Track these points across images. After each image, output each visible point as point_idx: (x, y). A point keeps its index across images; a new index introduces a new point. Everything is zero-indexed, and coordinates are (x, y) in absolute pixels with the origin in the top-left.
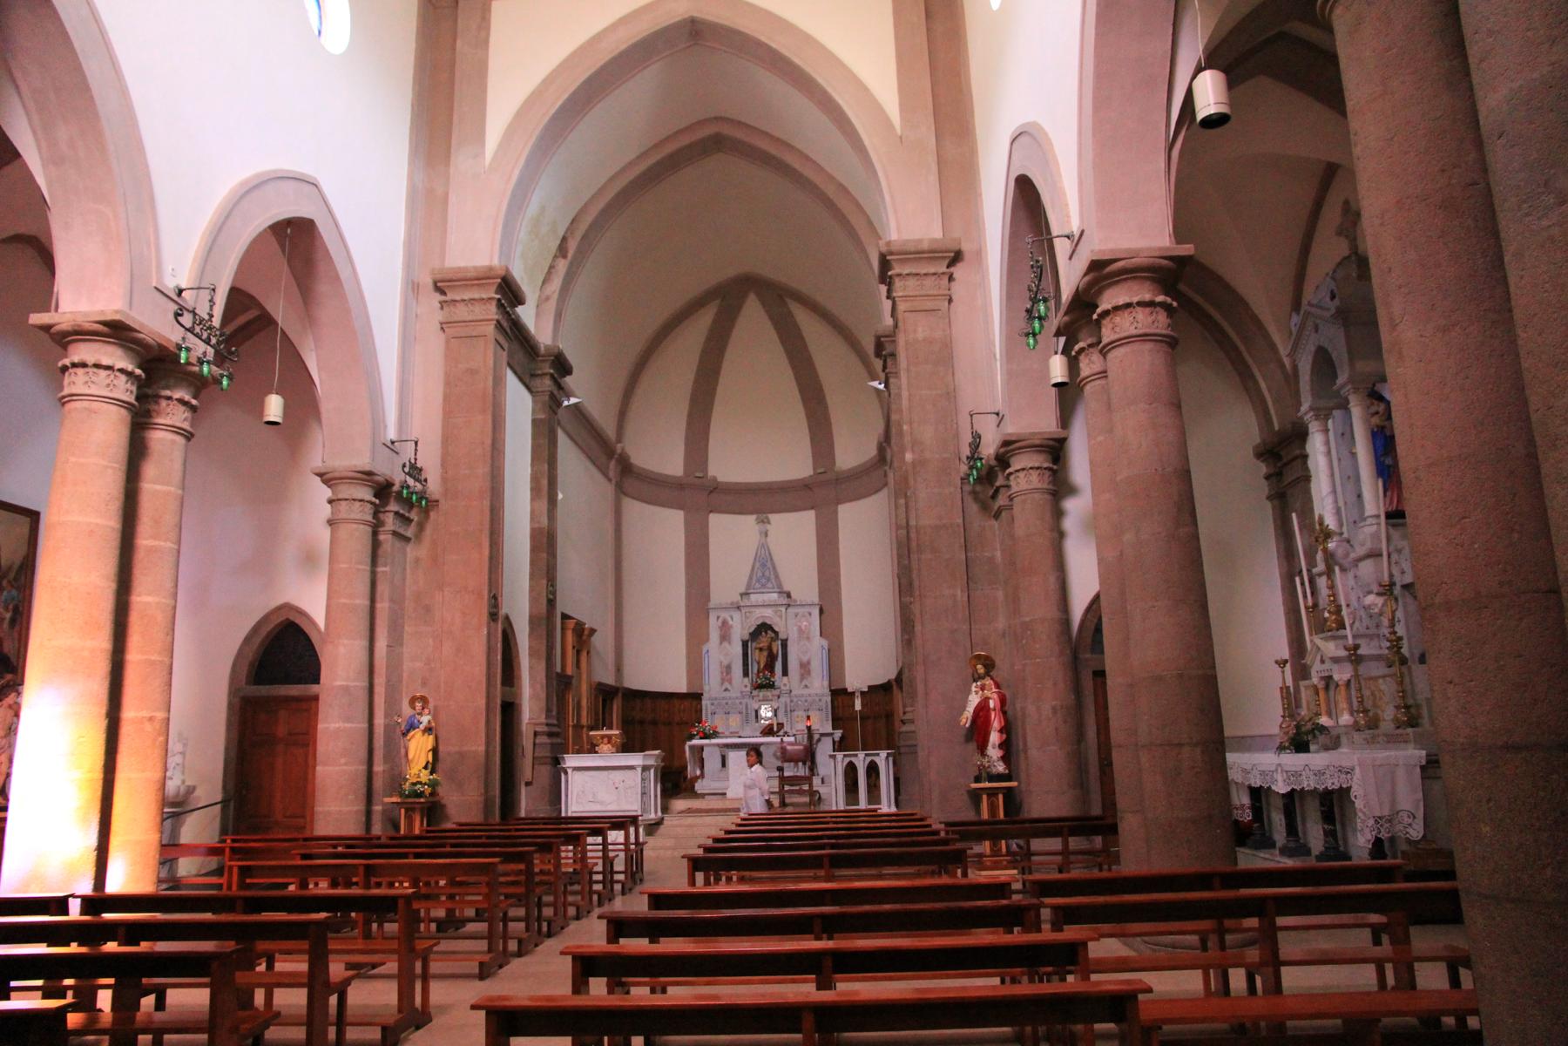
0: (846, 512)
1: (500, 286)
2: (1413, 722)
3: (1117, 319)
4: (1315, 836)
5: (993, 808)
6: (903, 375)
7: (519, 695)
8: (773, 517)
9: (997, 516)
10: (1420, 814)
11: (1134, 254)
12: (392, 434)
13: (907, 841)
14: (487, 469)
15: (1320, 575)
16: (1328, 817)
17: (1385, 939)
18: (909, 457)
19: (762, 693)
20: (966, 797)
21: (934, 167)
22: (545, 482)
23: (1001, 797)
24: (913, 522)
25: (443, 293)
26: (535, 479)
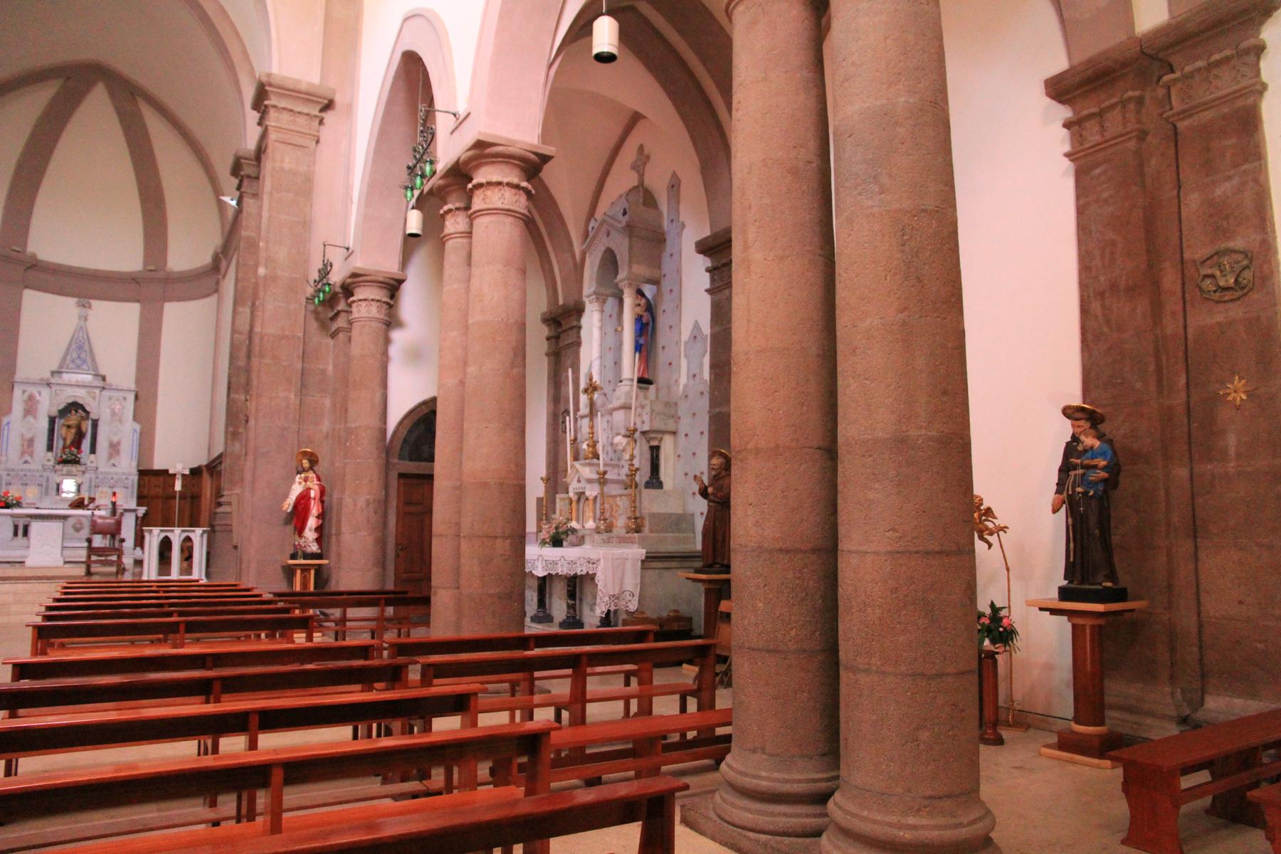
2: (638, 530)
3: (489, 193)
4: (559, 608)
5: (305, 584)
6: (266, 198)
8: (95, 303)
9: (334, 335)
11: (511, 143)
13: (220, 609)
15: (582, 417)
16: (572, 595)
17: (634, 681)
18: (261, 271)
19: (66, 468)
20: (280, 571)
21: (321, 21)
23: (313, 572)
24: (257, 329)
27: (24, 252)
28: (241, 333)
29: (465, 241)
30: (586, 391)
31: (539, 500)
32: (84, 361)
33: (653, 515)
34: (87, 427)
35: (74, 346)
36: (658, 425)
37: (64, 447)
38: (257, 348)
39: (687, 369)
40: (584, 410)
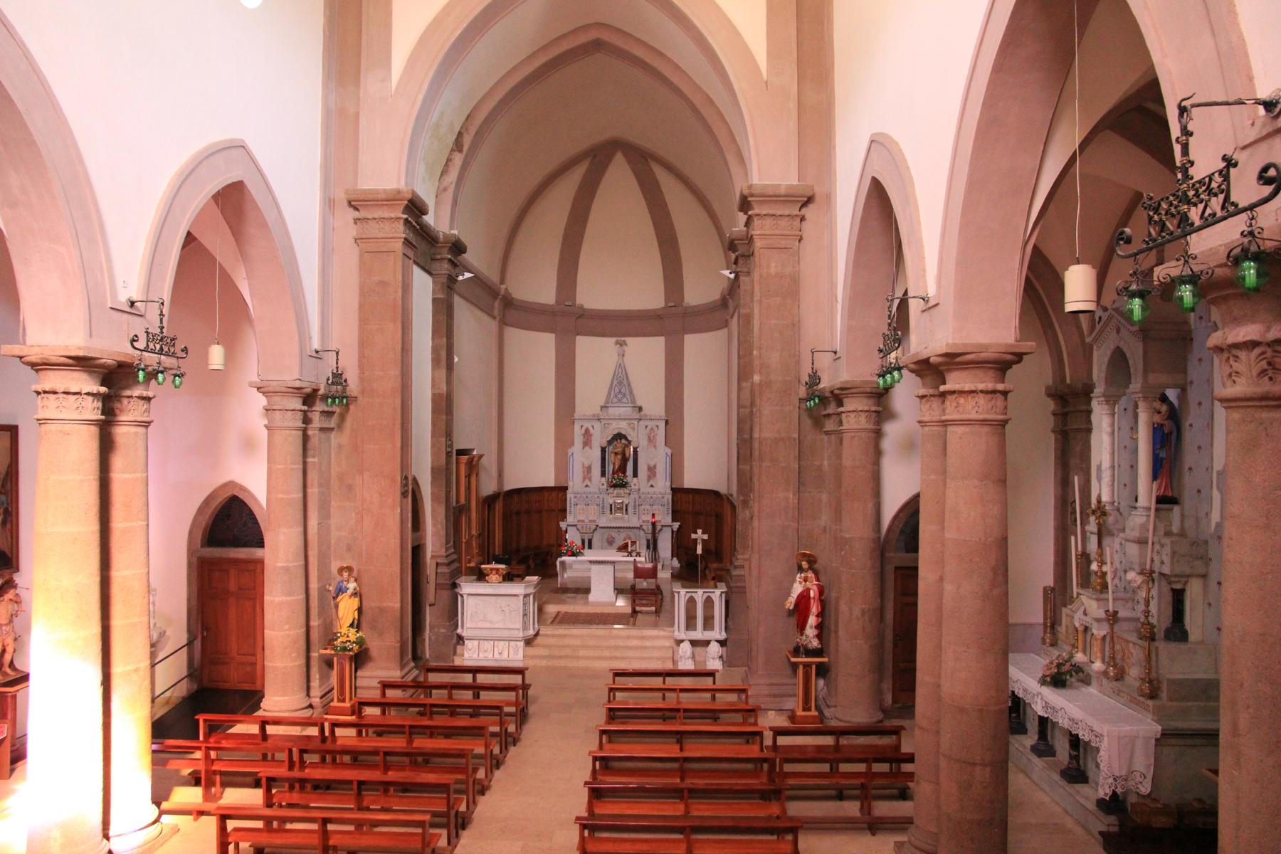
0: (693, 343)
1: (407, 206)
2: (1153, 695)
3: (962, 400)
7: (423, 537)
10: (1150, 777)
11: (985, 348)
12: (316, 344)
14: (398, 372)
18: (756, 378)
19: (617, 491)
22: (443, 354)
25: (356, 209)
26: (435, 350)
27: (574, 305)
28: (744, 407)
32: (624, 395)
33: (1172, 682)
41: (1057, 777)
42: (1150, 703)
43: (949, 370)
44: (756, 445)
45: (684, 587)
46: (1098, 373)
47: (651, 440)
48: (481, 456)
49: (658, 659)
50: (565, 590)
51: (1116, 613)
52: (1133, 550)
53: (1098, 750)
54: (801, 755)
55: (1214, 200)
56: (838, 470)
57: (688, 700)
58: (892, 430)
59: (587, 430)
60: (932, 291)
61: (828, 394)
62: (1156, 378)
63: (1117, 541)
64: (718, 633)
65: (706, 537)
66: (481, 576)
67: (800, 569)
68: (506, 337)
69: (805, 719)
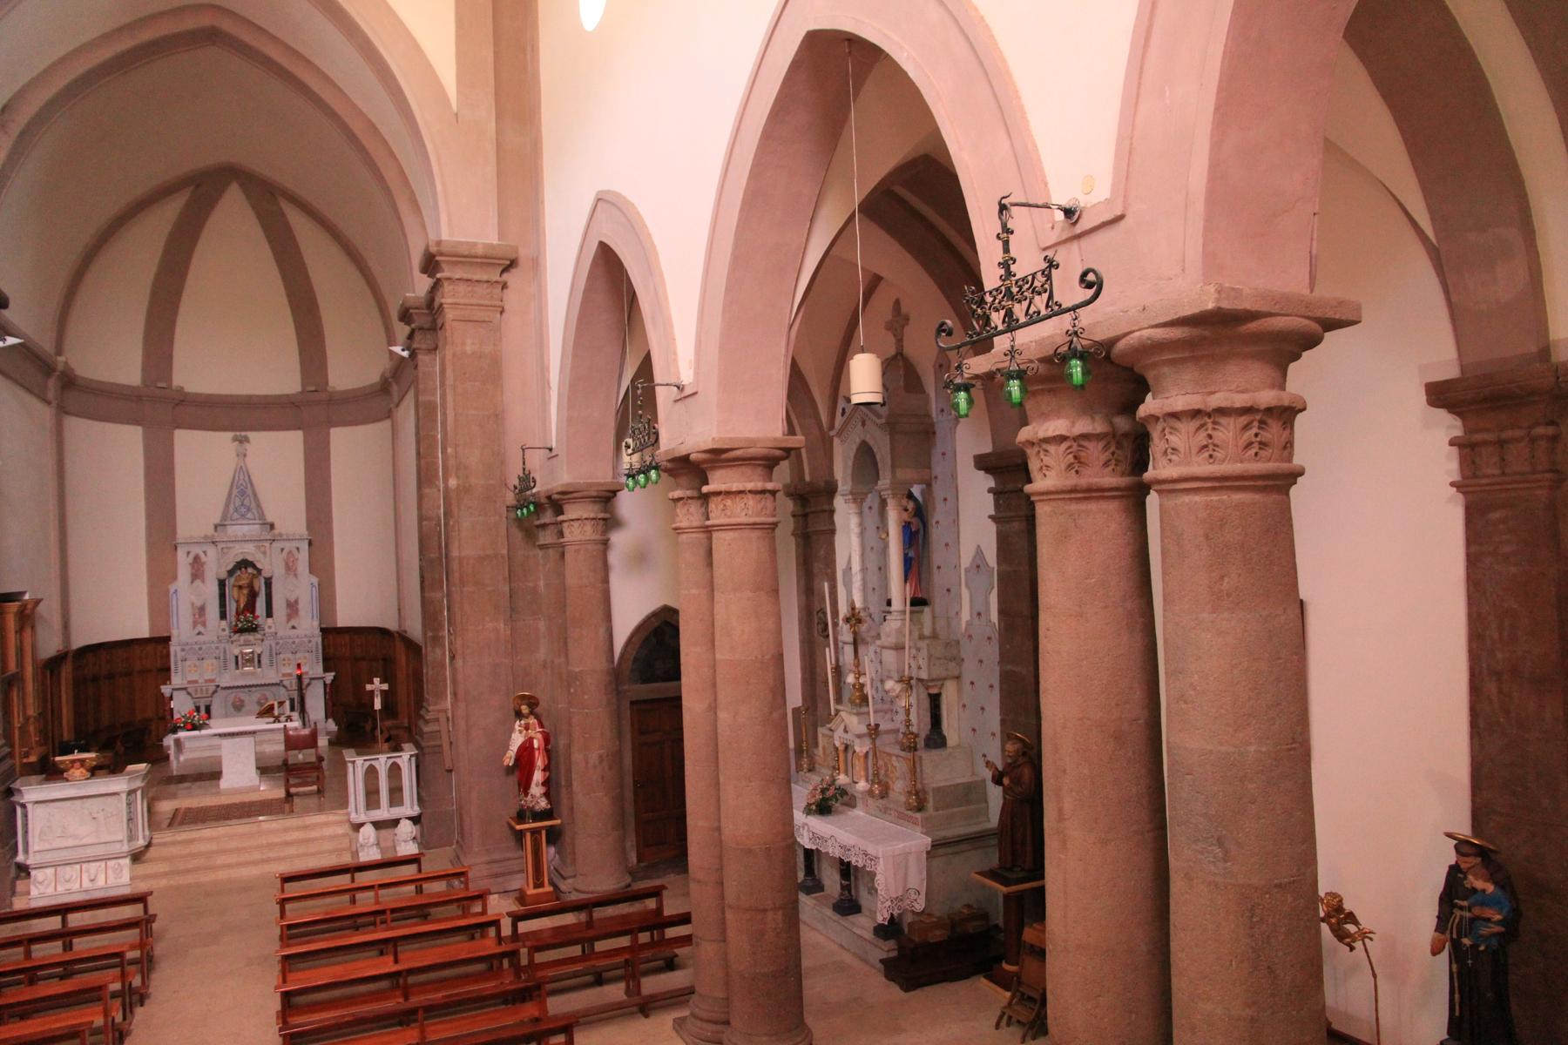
0: (340, 437)
3: (729, 502)
8: (253, 435)
11: (752, 442)
18: (453, 482)
27: (170, 387)
28: (429, 519)
29: (703, 536)
30: (847, 620)
31: (796, 711)
33: (938, 790)
34: (260, 585)
35: (235, 492)
36: (938, 671)
37: (238, 614)
38: (457, 575)
39: (973, 605)
40: (848, 637)
41: (829, 912)
42: (918, 815)
43: (713, 469)
44: (455, 566)
45: (359, 754)
46: (842, 471)
47: (290, 568)
48: (38, 602)
49: (331, 852)
50: (182, 779)
51: (877, 725)
52: (889, 657)
53: (872, 875)
54: (540, 943)
55: (1037, 298)
56: (562, 589)
57: (389, 898)
58: (620, 541)
59: (197, 558)
60: (686, 376)
61: (543, 500)
62: (904, 474)
63: (872, 649)
64: (410, 808)
65: (385, 687)
66: (50, 772)
67: (519, 715)
68: (67, 435)
69: (538, 899)
